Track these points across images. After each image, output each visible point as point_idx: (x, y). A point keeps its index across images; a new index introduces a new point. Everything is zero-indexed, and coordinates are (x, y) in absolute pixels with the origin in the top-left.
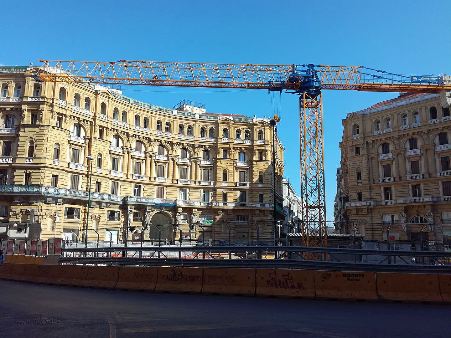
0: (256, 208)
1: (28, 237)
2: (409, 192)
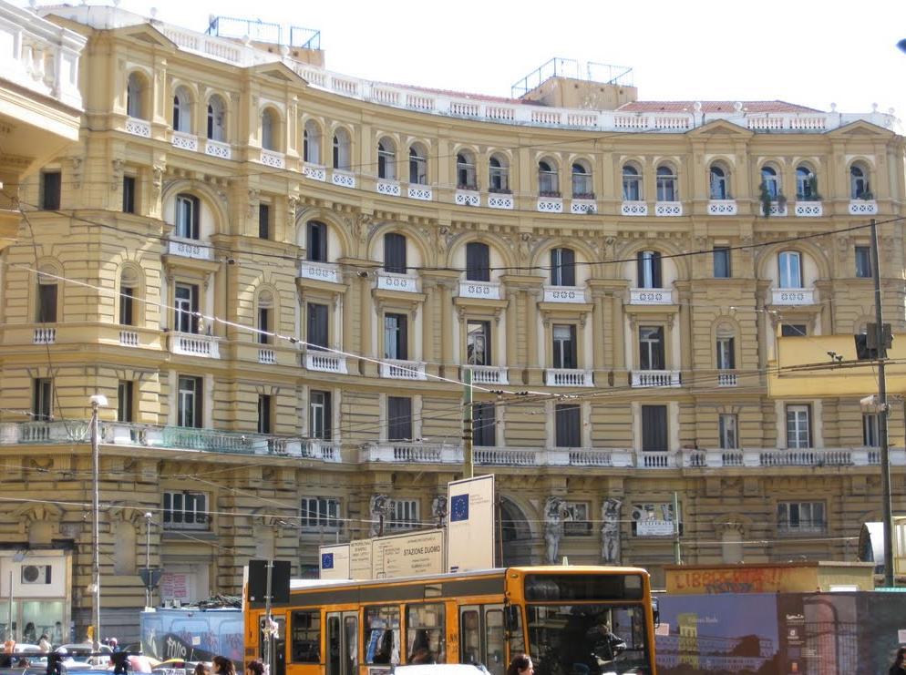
0: (851, 470)
1: (899, 631)
2: (590, 412)
